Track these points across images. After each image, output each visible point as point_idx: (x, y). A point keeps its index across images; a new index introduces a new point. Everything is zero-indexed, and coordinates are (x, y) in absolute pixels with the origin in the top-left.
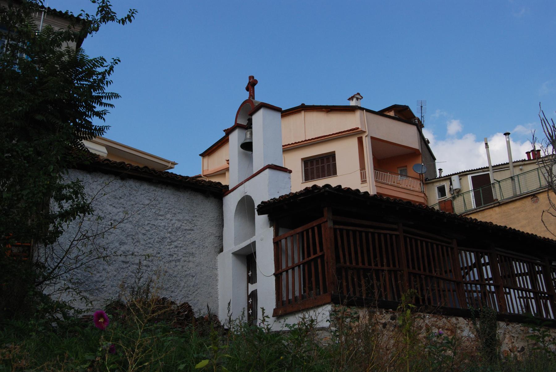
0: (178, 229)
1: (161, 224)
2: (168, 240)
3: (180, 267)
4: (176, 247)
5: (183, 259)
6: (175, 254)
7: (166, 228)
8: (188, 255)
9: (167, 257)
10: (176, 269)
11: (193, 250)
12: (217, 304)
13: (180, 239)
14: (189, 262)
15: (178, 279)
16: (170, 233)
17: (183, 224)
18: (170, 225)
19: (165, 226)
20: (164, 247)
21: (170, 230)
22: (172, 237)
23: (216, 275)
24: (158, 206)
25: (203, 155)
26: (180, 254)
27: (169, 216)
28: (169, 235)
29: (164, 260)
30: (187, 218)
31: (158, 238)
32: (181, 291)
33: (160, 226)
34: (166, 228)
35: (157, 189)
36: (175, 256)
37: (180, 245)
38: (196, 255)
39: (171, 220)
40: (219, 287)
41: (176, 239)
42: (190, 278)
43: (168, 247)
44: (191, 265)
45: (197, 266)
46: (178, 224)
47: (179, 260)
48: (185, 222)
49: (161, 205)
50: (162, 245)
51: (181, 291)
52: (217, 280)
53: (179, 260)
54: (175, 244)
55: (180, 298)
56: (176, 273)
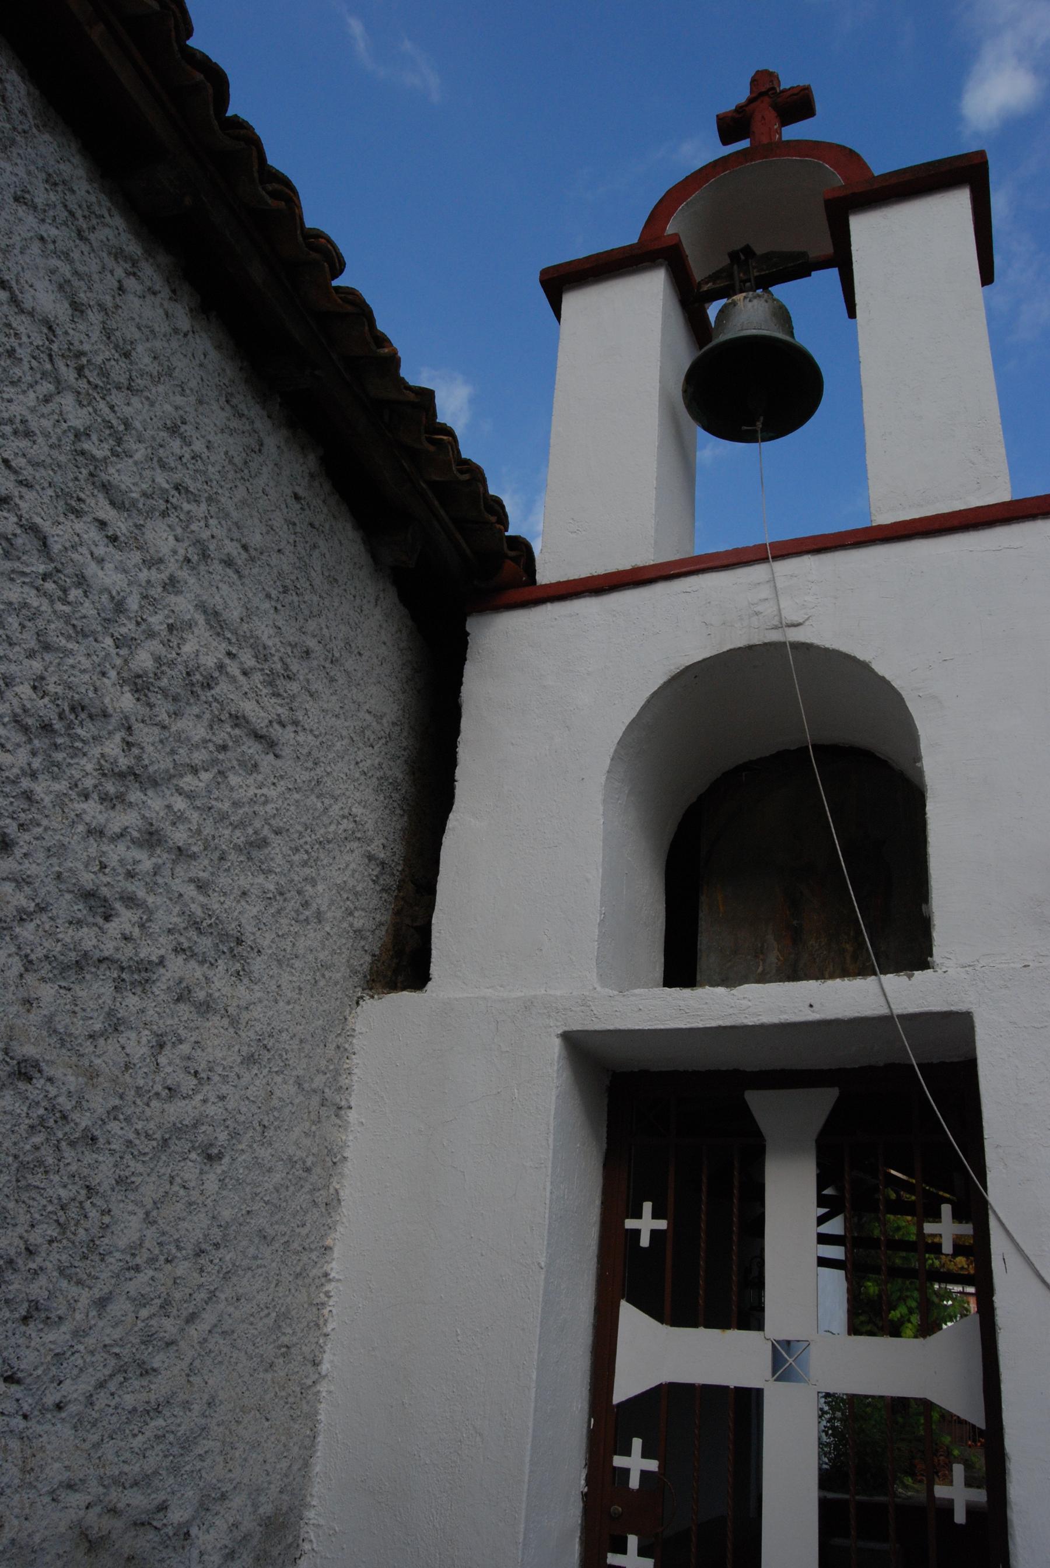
0: (199, 683)
1: (92, 569)
2: (113, 747)
3: (136, 1045)
4: (151, 838)
5: (176, 966)
6: (130, 901)
7: (127, 628)
8: (205, 944)
9: (65, 906)
10: (107, 1056)
11: (247, 915)
12: (312, 1417)
13: (188, 781)
14: (205, 1008)
15: (104, 1176)
16: (139, 685)
17: (233, 669)
18: (157, 621)
19: (120, 607)
20: (60, 801)
21: (143, 659)
22: (146, 735)
23: (332, 1159)
24: (117, 398)
25: (987, 276)
26: (167, 916)
27: (161, 537)
28: (127, 701)
29: (27, 932)
30: (264, 632)
31: (38, 685)
32: (102, 1303)
33: (81, 581)
34: (127, 628)
35: (147, 270)
36: (125, 919)
37: (179, 836)
38: (257, 965)
39: (172, 584)
40: (335, 1268)
41: (165, 764)
42: (190, 1171)
43: (92, 809)
44: (217, 1045)
45: (250, 1060)
46: (201, 647)
47: (139, 975)
48: (248, 659)
49: (134, 408)
50: (54, 770)
51: (102, 1303)
52: (333, 1203)
53: (139, 975)
54: (155, 804)
55: (86, 1384)
56: (99, 1102)
